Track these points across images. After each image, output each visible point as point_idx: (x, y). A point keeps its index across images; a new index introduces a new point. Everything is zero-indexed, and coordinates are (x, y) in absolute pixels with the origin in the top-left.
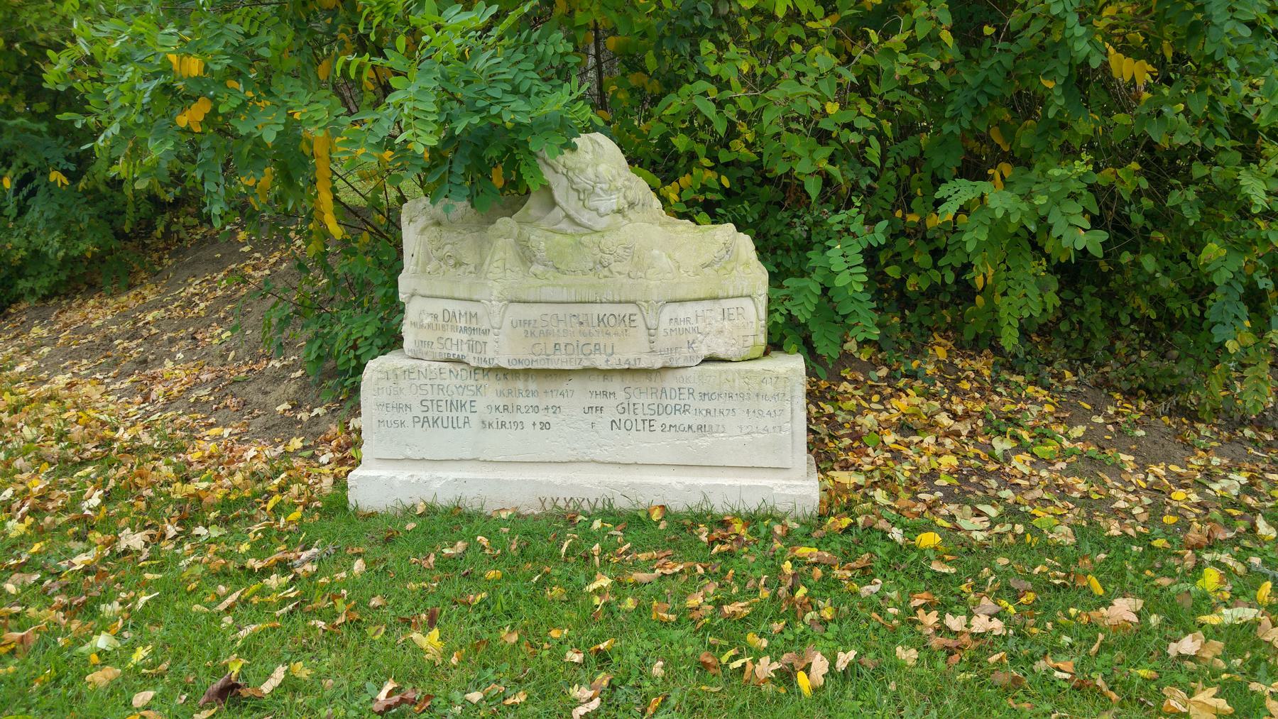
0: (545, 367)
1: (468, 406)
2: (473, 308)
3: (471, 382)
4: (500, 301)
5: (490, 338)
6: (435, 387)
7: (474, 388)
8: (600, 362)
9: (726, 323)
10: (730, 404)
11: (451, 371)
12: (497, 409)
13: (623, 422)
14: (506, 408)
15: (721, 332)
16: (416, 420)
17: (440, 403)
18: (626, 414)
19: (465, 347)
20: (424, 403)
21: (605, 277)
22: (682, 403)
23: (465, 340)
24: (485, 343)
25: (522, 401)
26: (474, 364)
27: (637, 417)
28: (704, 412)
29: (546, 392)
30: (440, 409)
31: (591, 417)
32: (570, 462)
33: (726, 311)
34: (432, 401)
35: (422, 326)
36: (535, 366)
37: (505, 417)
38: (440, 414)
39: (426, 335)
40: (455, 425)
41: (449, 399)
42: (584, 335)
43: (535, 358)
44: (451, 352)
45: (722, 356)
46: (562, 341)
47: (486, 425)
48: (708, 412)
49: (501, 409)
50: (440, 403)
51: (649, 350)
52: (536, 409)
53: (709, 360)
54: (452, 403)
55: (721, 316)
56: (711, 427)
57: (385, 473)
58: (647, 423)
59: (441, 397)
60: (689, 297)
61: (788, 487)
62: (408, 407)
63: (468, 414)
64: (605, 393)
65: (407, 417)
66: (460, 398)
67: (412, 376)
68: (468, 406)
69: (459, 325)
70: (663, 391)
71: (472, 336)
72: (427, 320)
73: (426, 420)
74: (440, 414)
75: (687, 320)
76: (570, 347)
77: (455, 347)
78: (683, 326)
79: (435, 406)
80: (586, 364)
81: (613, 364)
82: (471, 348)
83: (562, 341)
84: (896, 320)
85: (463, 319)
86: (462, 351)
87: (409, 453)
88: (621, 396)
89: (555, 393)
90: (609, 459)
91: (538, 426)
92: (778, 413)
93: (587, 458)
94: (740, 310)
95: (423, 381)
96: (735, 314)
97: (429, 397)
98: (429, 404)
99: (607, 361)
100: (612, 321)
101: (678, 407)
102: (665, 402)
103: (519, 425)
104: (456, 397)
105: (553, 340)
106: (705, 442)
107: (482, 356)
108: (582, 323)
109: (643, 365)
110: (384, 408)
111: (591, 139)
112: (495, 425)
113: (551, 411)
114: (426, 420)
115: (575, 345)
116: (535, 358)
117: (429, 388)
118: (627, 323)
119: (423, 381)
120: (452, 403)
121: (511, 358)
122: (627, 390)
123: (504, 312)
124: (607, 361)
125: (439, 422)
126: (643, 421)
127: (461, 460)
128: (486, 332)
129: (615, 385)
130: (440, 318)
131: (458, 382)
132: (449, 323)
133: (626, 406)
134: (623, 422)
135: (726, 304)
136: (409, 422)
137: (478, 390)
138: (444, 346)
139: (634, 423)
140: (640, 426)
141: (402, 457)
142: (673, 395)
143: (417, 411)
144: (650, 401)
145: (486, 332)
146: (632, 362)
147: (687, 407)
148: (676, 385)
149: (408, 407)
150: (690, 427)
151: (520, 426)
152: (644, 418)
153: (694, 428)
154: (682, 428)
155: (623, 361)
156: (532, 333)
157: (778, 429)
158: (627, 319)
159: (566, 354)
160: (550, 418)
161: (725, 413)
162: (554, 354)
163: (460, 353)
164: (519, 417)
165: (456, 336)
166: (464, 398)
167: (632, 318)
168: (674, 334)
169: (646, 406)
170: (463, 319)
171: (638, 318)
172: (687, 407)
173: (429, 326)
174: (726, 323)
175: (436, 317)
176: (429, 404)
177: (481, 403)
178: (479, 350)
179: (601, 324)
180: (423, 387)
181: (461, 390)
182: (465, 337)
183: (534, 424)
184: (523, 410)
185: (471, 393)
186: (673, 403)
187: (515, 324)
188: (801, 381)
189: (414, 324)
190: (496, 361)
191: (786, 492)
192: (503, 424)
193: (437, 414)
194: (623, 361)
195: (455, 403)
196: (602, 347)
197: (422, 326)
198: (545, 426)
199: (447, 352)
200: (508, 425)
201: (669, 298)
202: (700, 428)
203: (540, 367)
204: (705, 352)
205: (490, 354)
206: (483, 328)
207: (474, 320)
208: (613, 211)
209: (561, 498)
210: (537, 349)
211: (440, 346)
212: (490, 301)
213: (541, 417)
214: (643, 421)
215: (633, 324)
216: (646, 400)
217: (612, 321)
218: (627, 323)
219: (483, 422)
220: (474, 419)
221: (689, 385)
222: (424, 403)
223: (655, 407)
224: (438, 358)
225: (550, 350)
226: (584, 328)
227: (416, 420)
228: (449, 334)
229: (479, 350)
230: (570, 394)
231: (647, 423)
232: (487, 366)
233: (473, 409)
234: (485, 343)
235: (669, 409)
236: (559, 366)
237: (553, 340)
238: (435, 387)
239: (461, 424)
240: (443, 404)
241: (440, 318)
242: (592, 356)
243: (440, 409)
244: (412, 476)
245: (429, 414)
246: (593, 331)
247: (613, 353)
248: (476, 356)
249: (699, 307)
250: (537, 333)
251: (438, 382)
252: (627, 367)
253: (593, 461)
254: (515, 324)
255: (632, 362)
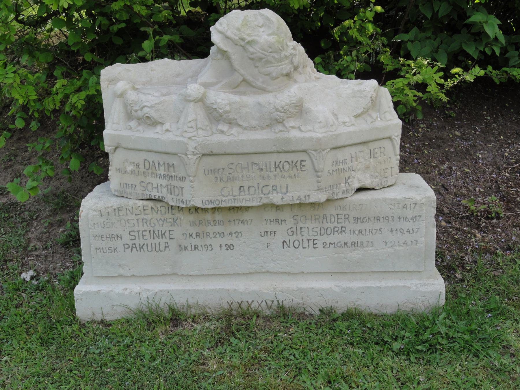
0: (233, 205)
1: (167, 234)
2: (171, 160)
3: (170, 216)
4: (195, 155)
5: (186, 184)
6: (140, 221)
7: (171, 220)
8: (277, 199)
9: (372, 160)
10: (378, 226)
11: (152, 208)
12: (191, 235)
13: (292, 242)
14: (198, 235)
15: (367, 168)
16: (126, 246)
17: (144, 233)
18: (295, 236)
19: (164, 190)
20: (132, 233)
21: (281, 131)
22: (340, 226)
23: (164, 185)
24: (182, 188)
25: (210, 229)
26: (172, 203)
27: (304, 238)
28: (357, 232)
29: (230, 221)
30: (145, 237)
31: (266, 240)
32: (250, 273)
33: (372, 151)
34: (138, 231)
35: (125, 172)
36: (224, 205)
37: (198, 242)
38: (145, 241)
39: (130, 179)
40: (158, 249)
41: (152, 229)
42: (263, 178)
43: (224, 199)
44: (153, 194)
45: (369, 187)
46: (246, 184)
47: (182, 248)
48: (360, 232)
49: (194, 235)
50: (144, 233)
51: (317, 188)
52: (222, 234)
53: (360, 190)
54: (154, 232)
55: (369, 156)
56: (362, 243)
57: (104, 288)
58: (311, 242)
59: (145, 228)
60: (347, 143)
61: (422, 285)
62: (119, 237)
63: (168, 240)
64: (277, 221)
65: (119, 244)
66: (160, 228)
67: (121, 213)
68: (167, 234)
69: (159, 172)
70: (325, 217)
71: (170, 182)
72: (130, 168)
73: (134, 246)
74: (145, 241)
75: (344, 162)
76: (252, 190)
77: (155, 190)
78: (341, 166)
79: (141, 235)
80: (265, 201)
81: (288, 199)
82: (170, 191)
83: (246, 184)
84: (336, 29)
85: (162, 168)
86: (163, 193)
87: (122, 272)
88: (290, 222)
89: (237, 222)
90: (281, 270)
91: (224, 248)
92: (415, 230)
93: (263, 270)
94: (382, 150)
95: (130, 216)
96: (379, 152)
97: (136, 228)
98: (136, 234)
99: (283, 198)
100: (287, 166)
101: (336, 229)
102: (326, 225)
103: (208, 247)
104: (157, 228)
105: (238, 184)
106: (356, 254)
107: (179, 197)
108: (262, 169)
109: (312, 200)
110: (100, 238)
111: (262, 15)
112: (189, 248)
113: (234, 236)
114: (134, 246)
115: (256, 186)
116: (224, 199)
117: (135, 221)
118: (299, 168)
119: (130, 216)
120: (154, 232)
121: (205, 199)
122: (295, 218)
123: (198, 164)
124: (283, 198)
125: (145, 247)
126: (309, 240)
127: (163, 275)
128: (182, 179)
129: (286, 215)
130: (142, 166)
131: (159, 216)
132: (150, 171)
133: (294, 230)
134: (292, 242)
135: (372, 146)
136: (120, 249)
137: (175, 222)
138: (146, 188)
139: (301, 242)
140: (306, 244)
141: (116, 275)
142: (333, 220)
143: (127, 239)
144: (314, 225)
145: (182, 179)
146: (303, 199)
147: (343, 229)
148: (334, 212)
149: (119, 237)
150: (345, 244)
151: (210, 248)
152: (309, 238)
153: (349, 244)
154: (339, 245)
155: (295, 198)
156: (221, 179)
157: (414, 242)
158: (298, 165)
159: (249, 194)
160: (233, 241)
161: (374, 232)
162: (239, 195)
163: (161, 195)
164: (209, 241)
165: (156, 181)
166: (164, 229)
167: (303, 163)
168: (335, 173)
169: (310, 229)
170: (162, 168)
171: (308, 163)
172: (343, 229)
173: (132, 172)
174: (372, 160)
175: (137, 165)
176: (136, 234)
177: (177, 232)
178: (177, 193)
179: (278, 170)
180: (130, 221)
181: (161, 222)
182: (164, 182)
183: (221, 246)
184: (212, 236)
185: (170, 224)
186: (332, 226)
187: (206, 172)
188: (433, 205)
189: (119, 170)
190: (192, 203)
191: (420, 289)
192: (196, 247)
193: (142, 242)
194: (295, 198)
195: (157, 232)
196: (278, 187)
197: (125, 172)
198: (230, 247)
199: (149, 193)
200: (200, 248)
201: (334, 146)
202: (354, 244)
203: (228, 205)
204: (357, 185)
205: (186, 196)
206: (180, 175)
207: (172, 169)
208: (283, 75)
209: (245, 300)
210: (225, 192)
211: (143, 189)
212: (186, 155)
213: (227, 240)
214: (309, 240)
215: (303, 168)
216: (310, 225)
217: (287, 166)
218: (299, 168)
219: (180, 246)
220: (173, 245)
221: (345, 212)
222: (132, 233)
223: (318, 230)
224: (141, 197)
225: (236, 192)
226: (264, 173)
227: (126, 246)
228: (150, 179)
229: (177, 193)
230: (249, 222)
231: (311, 242)
232: (184, 206)
233: (172, 237)
234: (182, 188)
235: (329, 231)
236: (244, 204)
237: (238, 184)
238: (140, 221)
239: (162, 247)
240: (147, 233)
241: (142, 166)
242: (270, 195)
243: (145, 237)
244: (126, 289)
245: (137, 242)
246: (271, 175)
247: (287, 192)
248: (175, 197)
249: (353, 150)
250: (225, 179)
251: (142, 216)
252: (298, 202)
253: (268, 272)
254: (206, 172)
255: (303, 199)
